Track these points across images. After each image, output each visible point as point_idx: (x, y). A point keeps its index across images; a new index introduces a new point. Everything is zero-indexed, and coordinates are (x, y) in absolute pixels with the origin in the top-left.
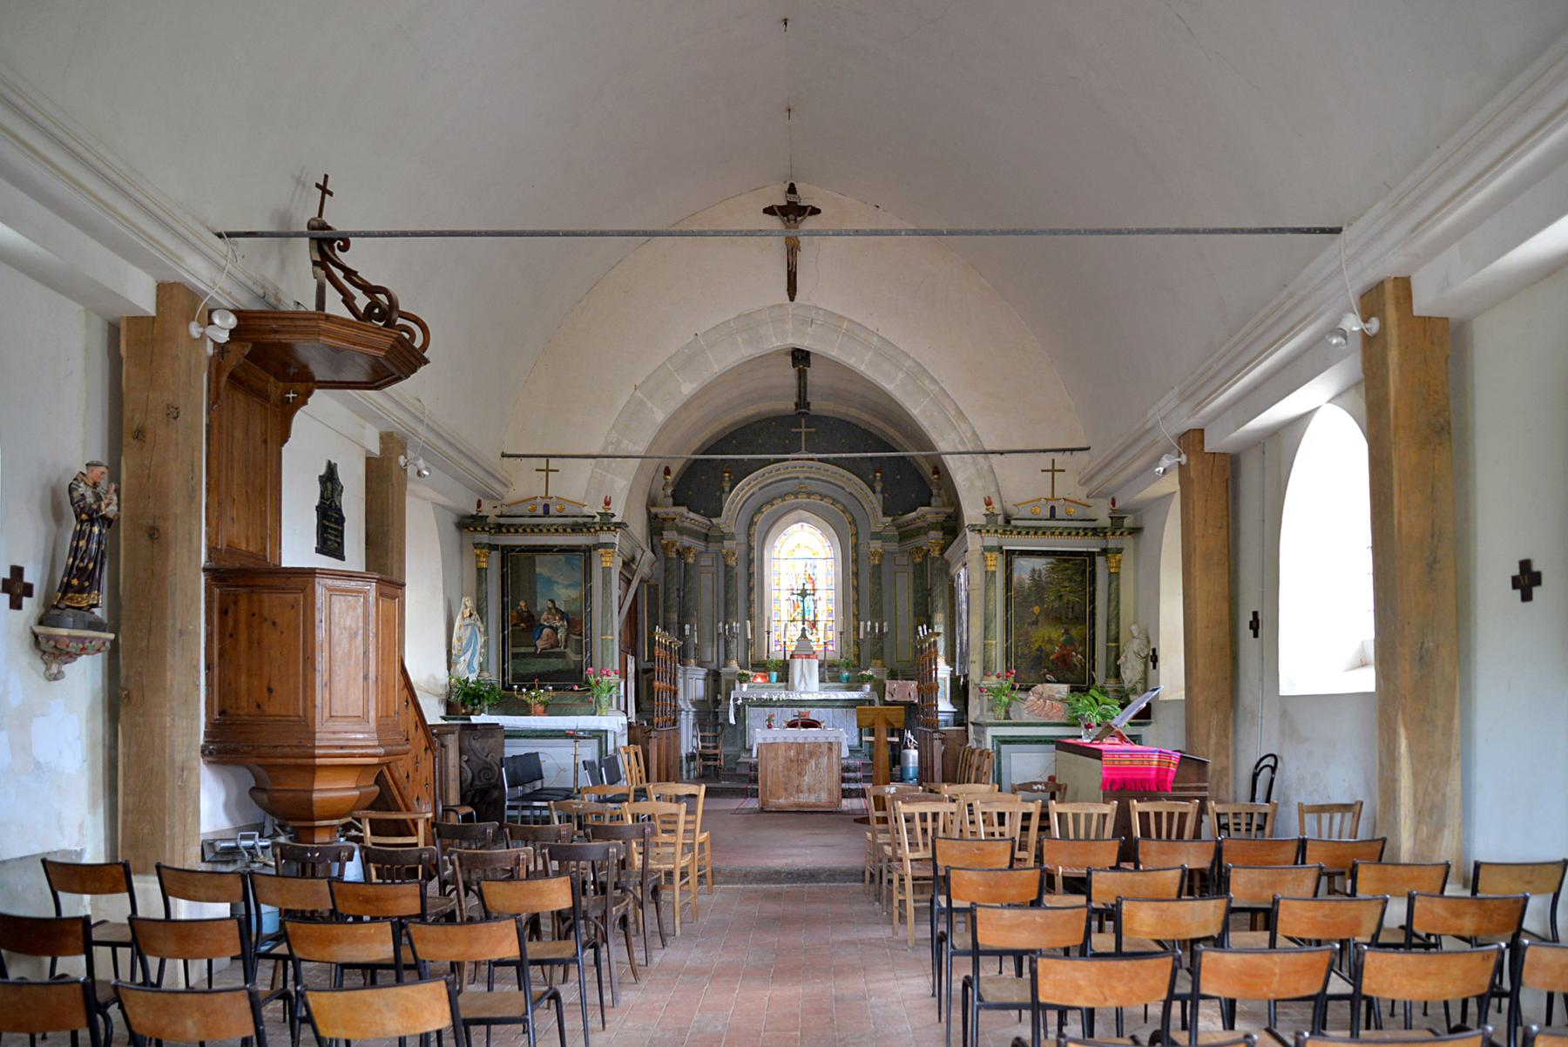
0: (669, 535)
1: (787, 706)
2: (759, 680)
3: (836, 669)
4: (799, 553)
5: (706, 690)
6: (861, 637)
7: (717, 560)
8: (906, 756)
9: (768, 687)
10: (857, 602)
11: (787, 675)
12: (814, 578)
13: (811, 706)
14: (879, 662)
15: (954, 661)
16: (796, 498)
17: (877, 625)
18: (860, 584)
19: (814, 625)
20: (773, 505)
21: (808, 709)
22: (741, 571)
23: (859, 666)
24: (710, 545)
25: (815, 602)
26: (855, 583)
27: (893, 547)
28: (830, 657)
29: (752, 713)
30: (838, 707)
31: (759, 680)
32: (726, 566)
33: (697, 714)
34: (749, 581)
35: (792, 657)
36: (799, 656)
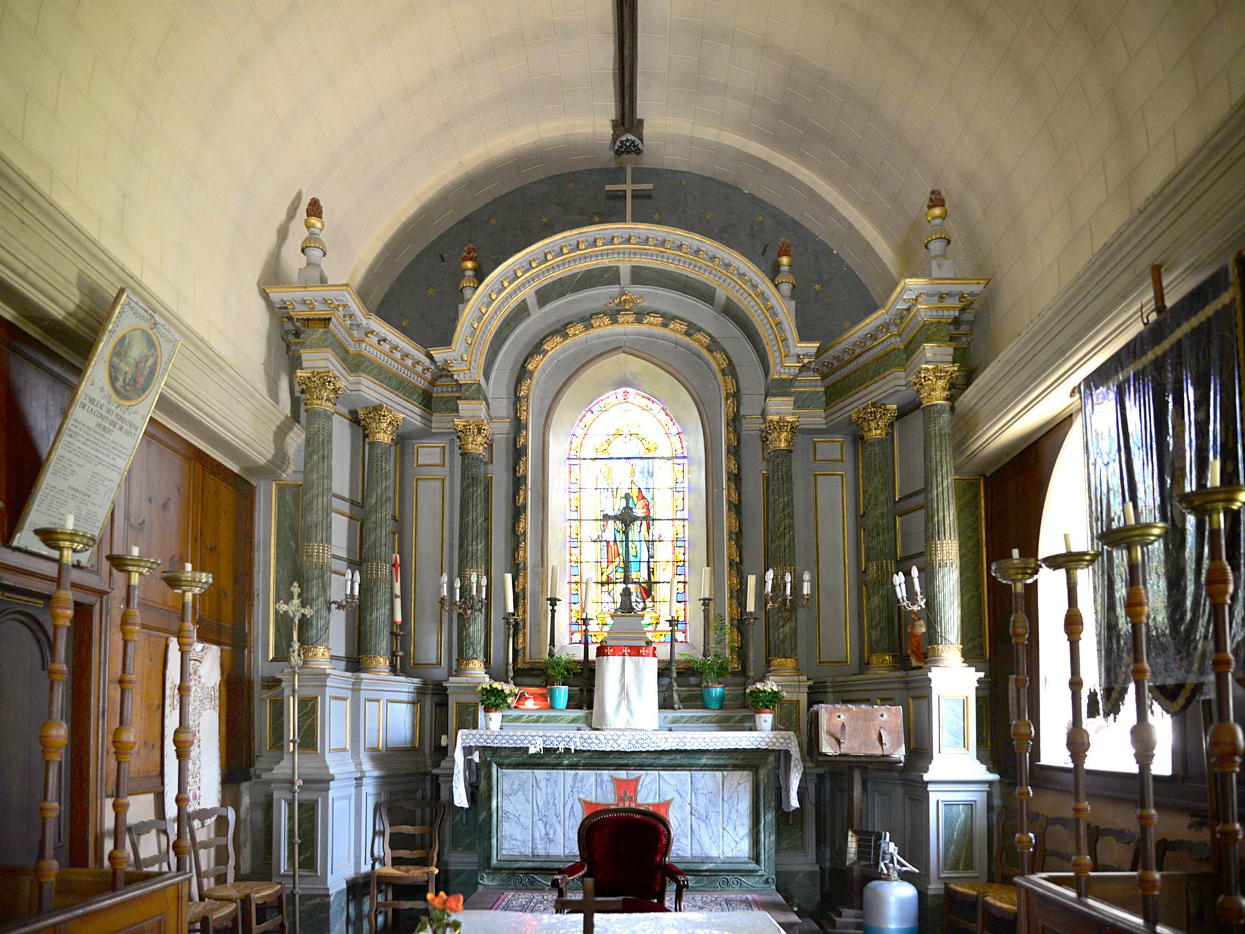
0: (316, 360)
1: (587, 766)
2: (530, 704)
3: (693, 680)
4: (619, 448)
5: (419, 723)
6: (751, 607)
7: (452, 452)
8: (879, 899)
9: (549, 720)
10: (738, 537)
11: (591, 692)
12: (648, 496)
13: (641, 767)
14: (790, 663)
15: (1211, 532)
16: (614, 321)
17: (788, 578)
18: (744, 499)
19: (648, 590)
20: (566, 336)
21: (636, 774)
22: (499, 474)
23: (744, 671)
24: (436, 417)
25: (650, 543)
26: (734, 498)
27: (816, 418)
28: (681, 653)
29: (507, 781)
30: (705, 767)
31: (530, 704)
32: (464, 455)
33: (385, 782)
34: (516, 493)
35: (601, 651)
36: (617, 651)
